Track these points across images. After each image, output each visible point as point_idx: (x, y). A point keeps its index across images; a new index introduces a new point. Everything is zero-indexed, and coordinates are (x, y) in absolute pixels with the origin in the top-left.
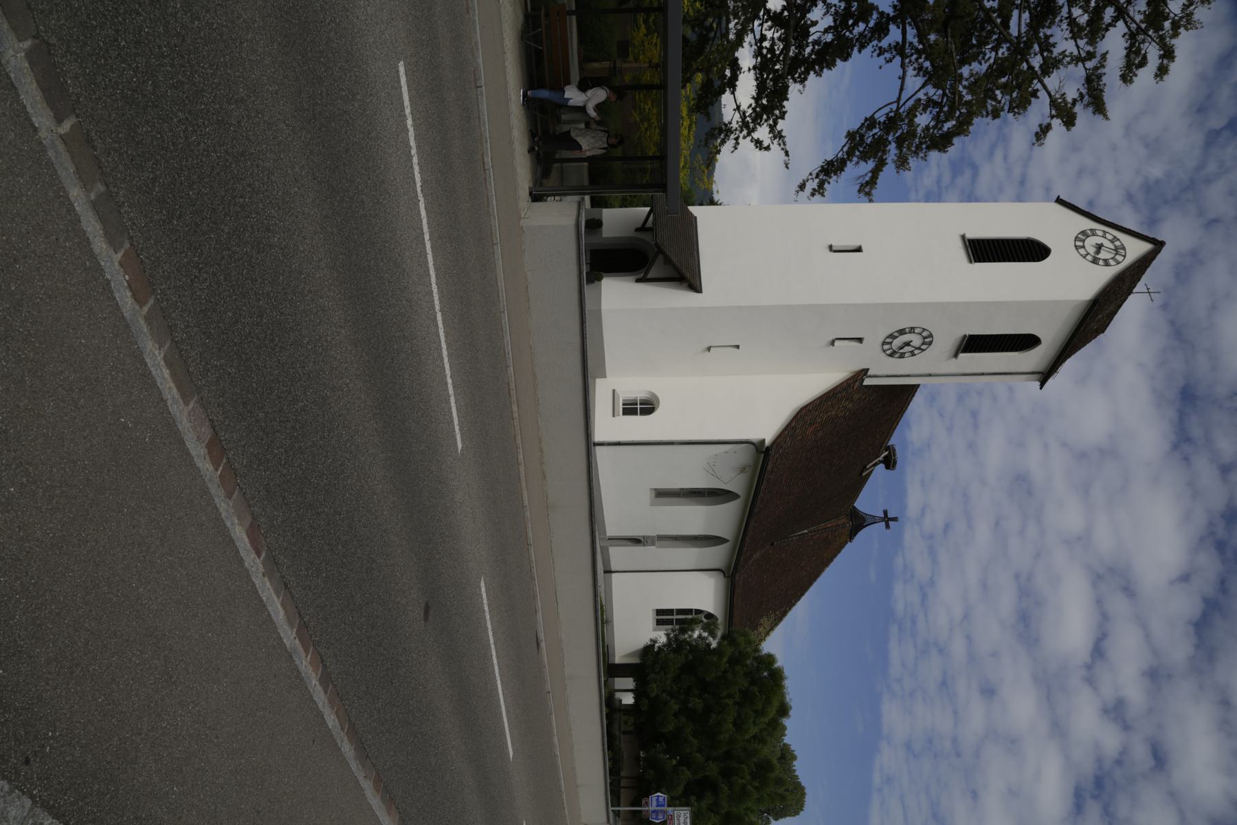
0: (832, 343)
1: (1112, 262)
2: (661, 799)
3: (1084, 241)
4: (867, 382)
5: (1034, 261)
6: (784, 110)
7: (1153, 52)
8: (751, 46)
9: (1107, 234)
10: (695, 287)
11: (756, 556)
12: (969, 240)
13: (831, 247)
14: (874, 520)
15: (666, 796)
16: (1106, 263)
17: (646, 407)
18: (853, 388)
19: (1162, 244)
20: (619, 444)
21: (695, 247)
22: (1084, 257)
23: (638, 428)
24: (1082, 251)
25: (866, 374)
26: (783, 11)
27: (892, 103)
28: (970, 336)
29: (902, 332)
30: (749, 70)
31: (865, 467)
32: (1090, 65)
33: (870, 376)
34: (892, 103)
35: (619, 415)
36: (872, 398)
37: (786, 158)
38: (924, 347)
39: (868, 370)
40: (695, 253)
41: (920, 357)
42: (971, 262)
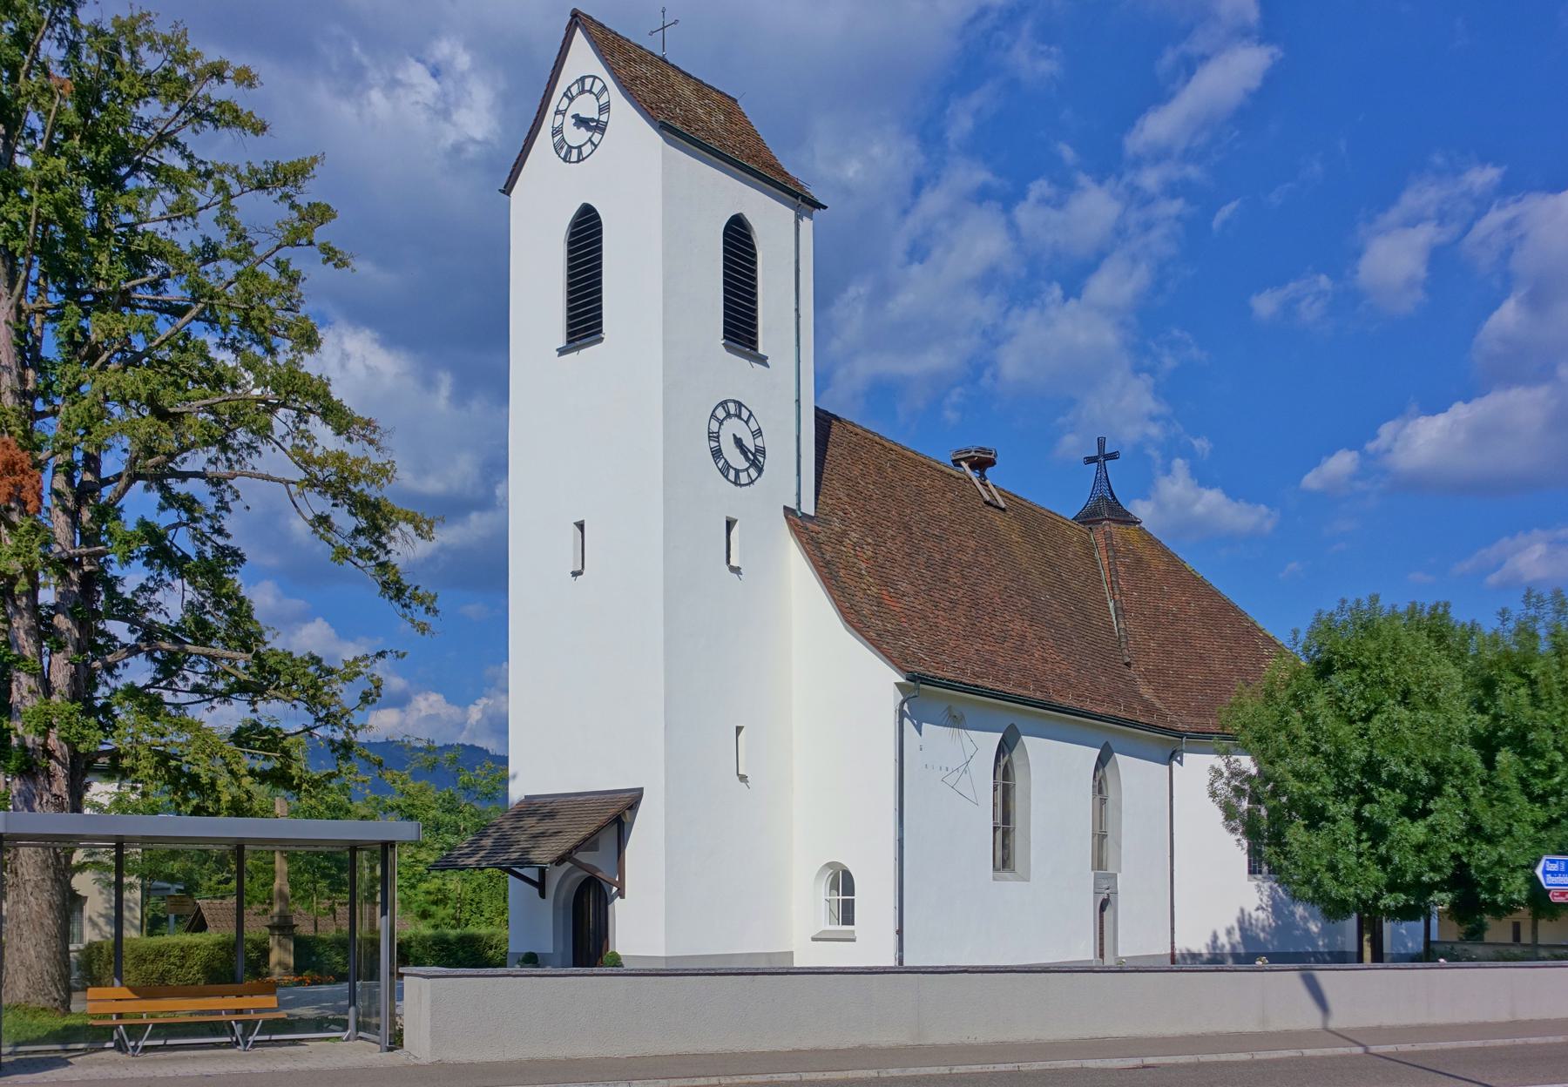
0: (736, 570)
1: (603, 100)
2: (1554, 867)
3: (570, 148)
4: (809, 508)
5: (600, 232)
6: (307, 658)
7: (217, 91)
8: (213, 707)
9: (560, 108)
10: (633, 800)
11: (1147, 692)
12: (569, 342)
13: (575, 574)
14: (1103, 480)
15: (1545, 858)
16: (604, 109)
17: (843, 882)
18: (818, 533)
19: (575, 15)
20: (900, 932)
21: (573, 798)
22: (596, 146)
23: (873, 898)
24: (586, 150)
25: (793, 511)
26: (155, 660)
27: (289, 493)
28: (725, 337)
29: (717, 453)
30: (255, 711)
31: (988, 503)
32: (235, 188)
33: (799, 504)
34: (289, 493)
35: (853, 932)
36: (846, 499)
37: (389, 656)
38: (745, 415)
39: (785, 508)
40: (621, 795)
41: (762, 420)
42: (601, 339)
